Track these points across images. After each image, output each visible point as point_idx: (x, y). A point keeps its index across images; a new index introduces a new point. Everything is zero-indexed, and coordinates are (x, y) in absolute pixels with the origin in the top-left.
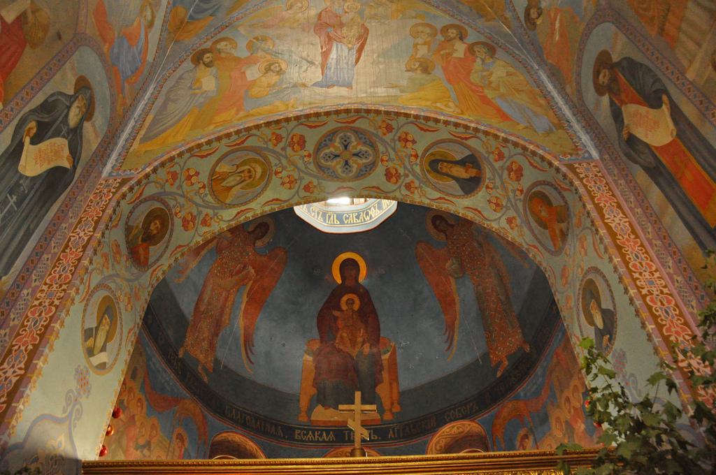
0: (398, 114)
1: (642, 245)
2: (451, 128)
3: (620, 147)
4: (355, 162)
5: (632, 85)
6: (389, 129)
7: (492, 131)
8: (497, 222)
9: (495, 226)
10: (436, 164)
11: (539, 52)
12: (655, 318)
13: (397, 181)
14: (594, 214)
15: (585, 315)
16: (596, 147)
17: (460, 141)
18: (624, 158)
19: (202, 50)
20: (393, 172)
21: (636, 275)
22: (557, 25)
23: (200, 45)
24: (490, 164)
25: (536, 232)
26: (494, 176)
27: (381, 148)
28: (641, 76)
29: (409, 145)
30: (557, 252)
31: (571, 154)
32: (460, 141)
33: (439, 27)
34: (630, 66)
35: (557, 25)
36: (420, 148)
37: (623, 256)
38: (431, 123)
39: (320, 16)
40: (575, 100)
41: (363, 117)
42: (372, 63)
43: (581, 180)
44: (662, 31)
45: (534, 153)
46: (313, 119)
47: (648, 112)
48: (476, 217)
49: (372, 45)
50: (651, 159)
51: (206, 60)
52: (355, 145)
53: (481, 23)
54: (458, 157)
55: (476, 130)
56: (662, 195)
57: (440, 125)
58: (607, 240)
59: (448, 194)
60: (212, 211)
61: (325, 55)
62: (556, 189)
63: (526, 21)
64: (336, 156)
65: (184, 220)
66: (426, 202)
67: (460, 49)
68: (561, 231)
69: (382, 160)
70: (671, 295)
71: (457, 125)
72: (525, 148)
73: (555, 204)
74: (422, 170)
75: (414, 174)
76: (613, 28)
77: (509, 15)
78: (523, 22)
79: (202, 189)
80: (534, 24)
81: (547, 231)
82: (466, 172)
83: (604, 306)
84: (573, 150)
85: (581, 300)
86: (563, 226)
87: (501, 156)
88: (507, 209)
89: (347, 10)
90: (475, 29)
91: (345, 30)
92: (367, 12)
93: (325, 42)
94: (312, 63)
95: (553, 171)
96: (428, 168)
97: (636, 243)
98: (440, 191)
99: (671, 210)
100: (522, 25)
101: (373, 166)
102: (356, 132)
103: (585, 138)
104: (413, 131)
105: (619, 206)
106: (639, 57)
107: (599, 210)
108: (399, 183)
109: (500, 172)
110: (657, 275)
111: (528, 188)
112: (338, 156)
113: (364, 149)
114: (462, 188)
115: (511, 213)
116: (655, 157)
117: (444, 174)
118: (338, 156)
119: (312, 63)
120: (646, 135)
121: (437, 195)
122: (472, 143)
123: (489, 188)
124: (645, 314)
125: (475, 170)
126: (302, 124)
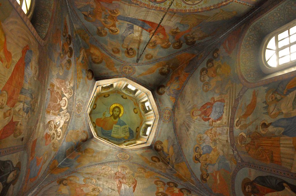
19: (62, 179)
22: (218, 177)
23: (62, 177)
28: (268, 181)
33: (166, 183)
34: (262, 180)
35: (218, 177)
39: (116, 174)
42: (141, 192)
44: (272, 161)
49: (139, 186)
51: (64, 183)
53: (182, 182)
63: (201, 180)
67: (176, 190)
77: (193, 179)
78: (200, 181)
80: (206, 180)
92: (136, 174)
94: (114, 190)
106: (264, 174)
119: (114, 190)
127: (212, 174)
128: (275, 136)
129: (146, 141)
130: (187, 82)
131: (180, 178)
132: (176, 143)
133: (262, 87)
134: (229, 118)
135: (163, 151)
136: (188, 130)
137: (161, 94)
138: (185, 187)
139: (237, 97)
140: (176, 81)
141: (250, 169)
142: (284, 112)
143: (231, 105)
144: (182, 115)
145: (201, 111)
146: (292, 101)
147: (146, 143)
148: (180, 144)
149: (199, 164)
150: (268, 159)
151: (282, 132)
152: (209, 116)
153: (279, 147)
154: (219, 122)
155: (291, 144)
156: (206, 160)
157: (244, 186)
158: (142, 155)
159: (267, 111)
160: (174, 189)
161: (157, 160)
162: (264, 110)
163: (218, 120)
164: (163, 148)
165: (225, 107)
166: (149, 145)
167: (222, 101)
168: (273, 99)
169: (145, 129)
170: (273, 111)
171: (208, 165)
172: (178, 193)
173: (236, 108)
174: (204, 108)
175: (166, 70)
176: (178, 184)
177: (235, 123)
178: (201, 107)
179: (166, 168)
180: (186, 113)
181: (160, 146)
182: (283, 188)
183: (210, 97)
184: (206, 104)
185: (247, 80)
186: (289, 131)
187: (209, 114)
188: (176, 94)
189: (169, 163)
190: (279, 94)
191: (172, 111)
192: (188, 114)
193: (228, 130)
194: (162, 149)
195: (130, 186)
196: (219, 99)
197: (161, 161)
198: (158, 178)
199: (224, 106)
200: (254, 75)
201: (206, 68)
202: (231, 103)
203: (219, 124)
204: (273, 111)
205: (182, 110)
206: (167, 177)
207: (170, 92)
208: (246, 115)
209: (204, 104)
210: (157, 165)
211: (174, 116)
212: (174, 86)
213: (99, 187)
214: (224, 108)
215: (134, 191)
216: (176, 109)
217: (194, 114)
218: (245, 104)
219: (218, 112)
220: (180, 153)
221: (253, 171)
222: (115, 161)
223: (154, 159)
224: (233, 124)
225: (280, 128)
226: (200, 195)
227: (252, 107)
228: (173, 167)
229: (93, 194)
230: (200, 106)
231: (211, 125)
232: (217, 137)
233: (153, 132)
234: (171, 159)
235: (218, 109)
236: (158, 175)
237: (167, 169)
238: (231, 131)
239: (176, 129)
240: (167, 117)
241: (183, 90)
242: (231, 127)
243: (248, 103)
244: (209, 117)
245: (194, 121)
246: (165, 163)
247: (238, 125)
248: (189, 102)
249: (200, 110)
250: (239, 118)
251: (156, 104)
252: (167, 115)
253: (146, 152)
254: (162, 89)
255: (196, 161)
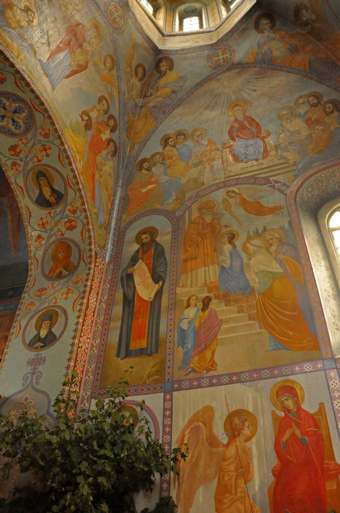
0: (59, 137)
1: (92, 321)
2: (71, 175)
3: (123, 272)
4: (8, 122)
5: (154, 259)
6: (46, 136)
7: (85, 199)
8: (33, 232)
9: (29, 230)
10: (41, 175)
11: (128, 182)
12: (76, 360)
13: (13, 155)
14: (88, 289)
15: (37, 320)
16: (111, 256)
17: (66, 184)
18: (119, 278)
20: (18, 150)
21: (82, 335)
22: (150, 187)
24: (65, 208)
25: (46, 257)
26: (59, 214)
27: (29, 136)
29: (44, 153)
30: (48, 277)
31: (100, 249)
32: (66, 184)
33: (111, 112)
35: (150, 187)
36: (45, 161)
37: (84, 321)
38: (66, 161)
39: (79, 24)
40: (123, 224)
41: (43, 115)
43: (95, 266)
44: (185, 261)
45: (89, 231)
46: (23, 83)
47: (149, 278)
48: (25, 216)
50: (131, 294)
52: (21, 118)
53: (124, 134)
54: (56, 187)
55: (80, 190)
56: (121, 313)
57: (68, 168)
58: (84, 307)
59: (27, 191)
60: (22, 170)
61: (59, 50)
62: (80, 255)
63: (140, 161)
64: (14, 121)
65: (68, 229)
66: (12, 180)
67: (106, 135)
68: (61, 273)
69: (21, 140)
70: (86, 354)
71: (75, 177)
72: (88, 224)
73: (72, 258)
74: (32, 168)
75: (26, 164)
76: (170, 229)
77: (136, 148)
79: (36, 159)
80: (141, 170)
81: (52, 263)
82: (50, 196)
83: (53, 330)
84: (102, 246)
85: (41, 313)
86: (65, 273)
87: (74, 212)
88: (45, 232)
89: (91, 43)
90: (120, 134)
91: (79, 50)
93: (65, 42)
94: (49, 44)
95: (88, 248)
96: (36, 172)
97: (91, 318)
98: (26, 184)
99: (119, 324)
100: (136, 160)
101: (12, 135)
102: (30, 115)
103: (110, 247)
104: (54, 152)
105: (97, 294)
107: (91, 289)
108: (13, 157)
109: (64, 216)
110: (88, 340)
111: (67, 238)
112: (13, 119)
113: (22, 124)
114: (37, 199)
115: (45, 235)
116: (134, 296)
117: (39, 182)
118: (13, 119)
119: (49, 44)
120: (139, 285)
121: (22, 185)
122: (71, 192)
123: (50, 214)
124: (74, 356)
125: (54, 201)
126: (15, 76)
127: (152, 176)
128: (218, 257)
129: (166, 33)
130: (290, 71)
131: (129, 128)
132: (180, 95)
133: (289, 219)
134: (238, 175)
135: (159, 78)
136: (207, 108)
137: (257, 26)
138: (117, 144)
139: (271, 179)
140: (289, 49)
141: (171, 233)
142: (252, 262)
143: (260, 172)
144: (229, 85)
145: (244, 119)
146: (267, 270)
147: (163, 36)
148: (180, 103)
149: (160, 149)
150: (187, 255)
151: (224, 265)
152: (238, 136)
153: (205, 266)
154: (231, 158)
155: (210, 279)
156: (170, 158)
157: (147, 232)
158: (135, 46)
159: (252, 236)
160: (106, 132)
161: (140, 75)
162: (254, 231)
163: (234, 156)
164: (164, 75)
165: (255, 163)
166: (160, 47)
167: (266, 154)
168: (271, 241)
169: (192, 10)
170: (251, 244)
171: (163, 164)
172: (104, 140)
173: (254, 183)
174: (249, 123)
175: (305, 19)
176: (118, 131)
177: (232, 189)
178: (251, 118)
179: (135, 97)
180: (234, 92)
181: (166, 69)
182: (156, 282)
183: (271, 128)
184: (258, 124)
185: (302, 187)
186: (226, 274)
187: (241, 136)
188: (263, 59)
189: (145, 96)
190: (277, 248)
191: (230, 64)
192: (234, 98)
193: (219, 179)
194: (162, 74)
195: (72, 63)
196: (268, 146)
197: (143, 82)
198: (111, 95)
199: (257, 160)
200: (313, 196)
201: (322, 103)
202: (263, 171)
203: (227, 160)
204: (251, 244)
205: (238, 82)
206: (120, 108)
207: (265, 44)
208: (244, 203)
209: (257, 120)
210: (132, 81)
211: (223, 72)
212: (278, 48)
213: (36, 15)
214: (254, 161)
215: (68, 77)
216: (237, 71)
217: (236, 109)
218: (262, 197)
219: (246, 152)
220: (165, 110)
221: (168, 238)
222: (98, 6)
223: (140, 70)
224: (229, 186)
225: (229, 261)
226: (118, 170)
227: (258, 210)
228: (141, 107)
229: (18, 18)
230: (252, 113)
231: (224, 146)
232: (207, 163)
233: (186, 41)
234: (152, 97)
235: (251, 150)
236: (115, 94)
237: (135, 100)
238: (218, 187)
239: (202, 85)
240: (218, 58)
241: (274, 69)
242: (225, 184)
243: (263, 202)
244: (236, 138)
245: (225, 114)
246: (142, 90)
247: (229, 194)
248: (255, 91)
249: (245, 117)
250: (239, 194)
251: (236, 25)
252: (221, 57)
253: (145, 48)
254: (266, 24)
255: (163, 143)
